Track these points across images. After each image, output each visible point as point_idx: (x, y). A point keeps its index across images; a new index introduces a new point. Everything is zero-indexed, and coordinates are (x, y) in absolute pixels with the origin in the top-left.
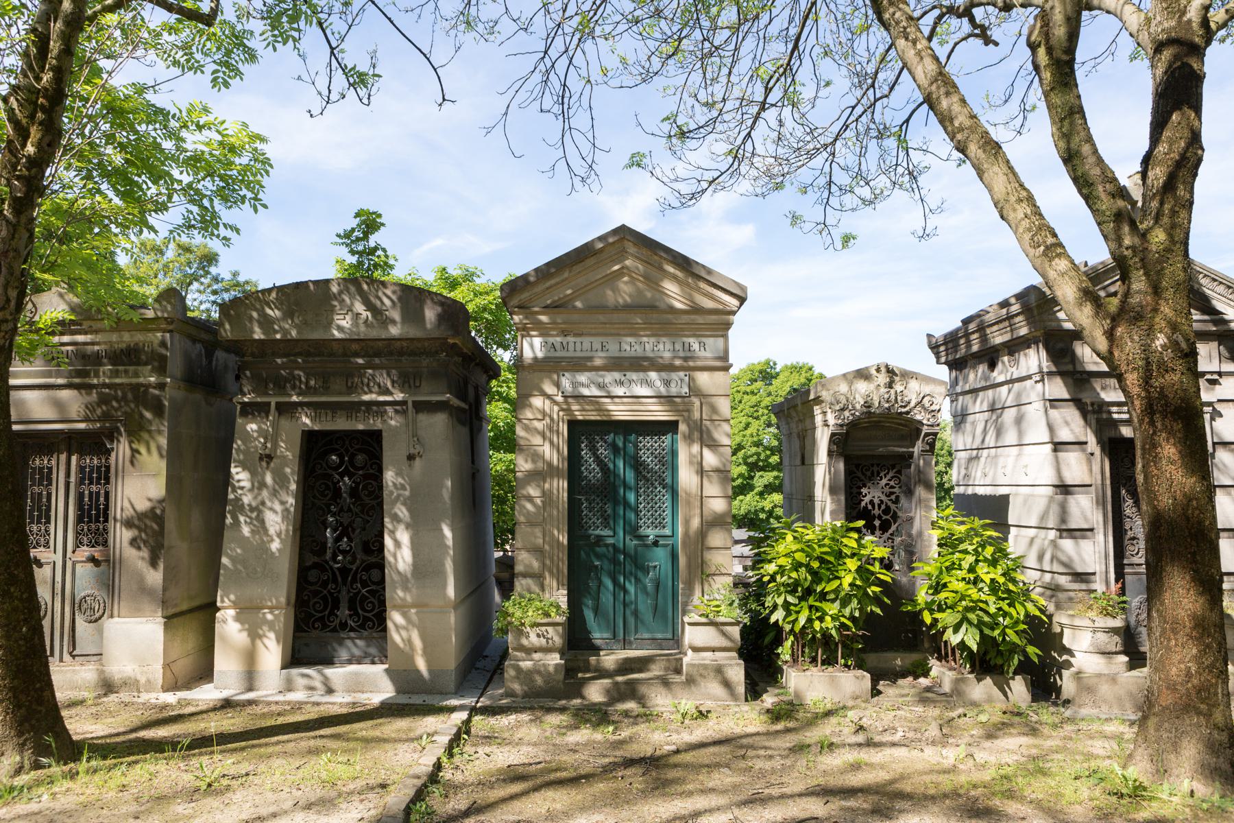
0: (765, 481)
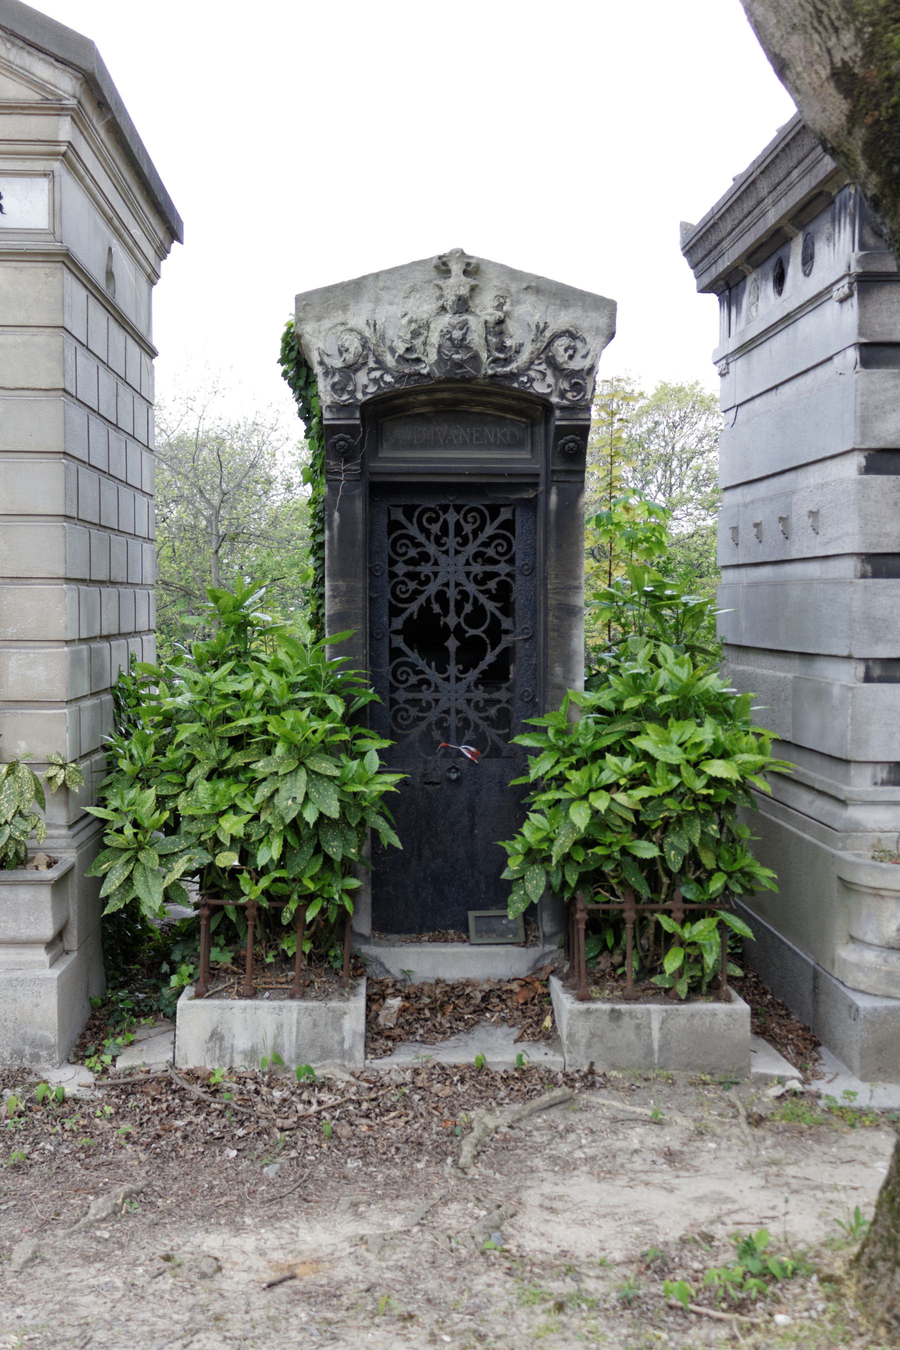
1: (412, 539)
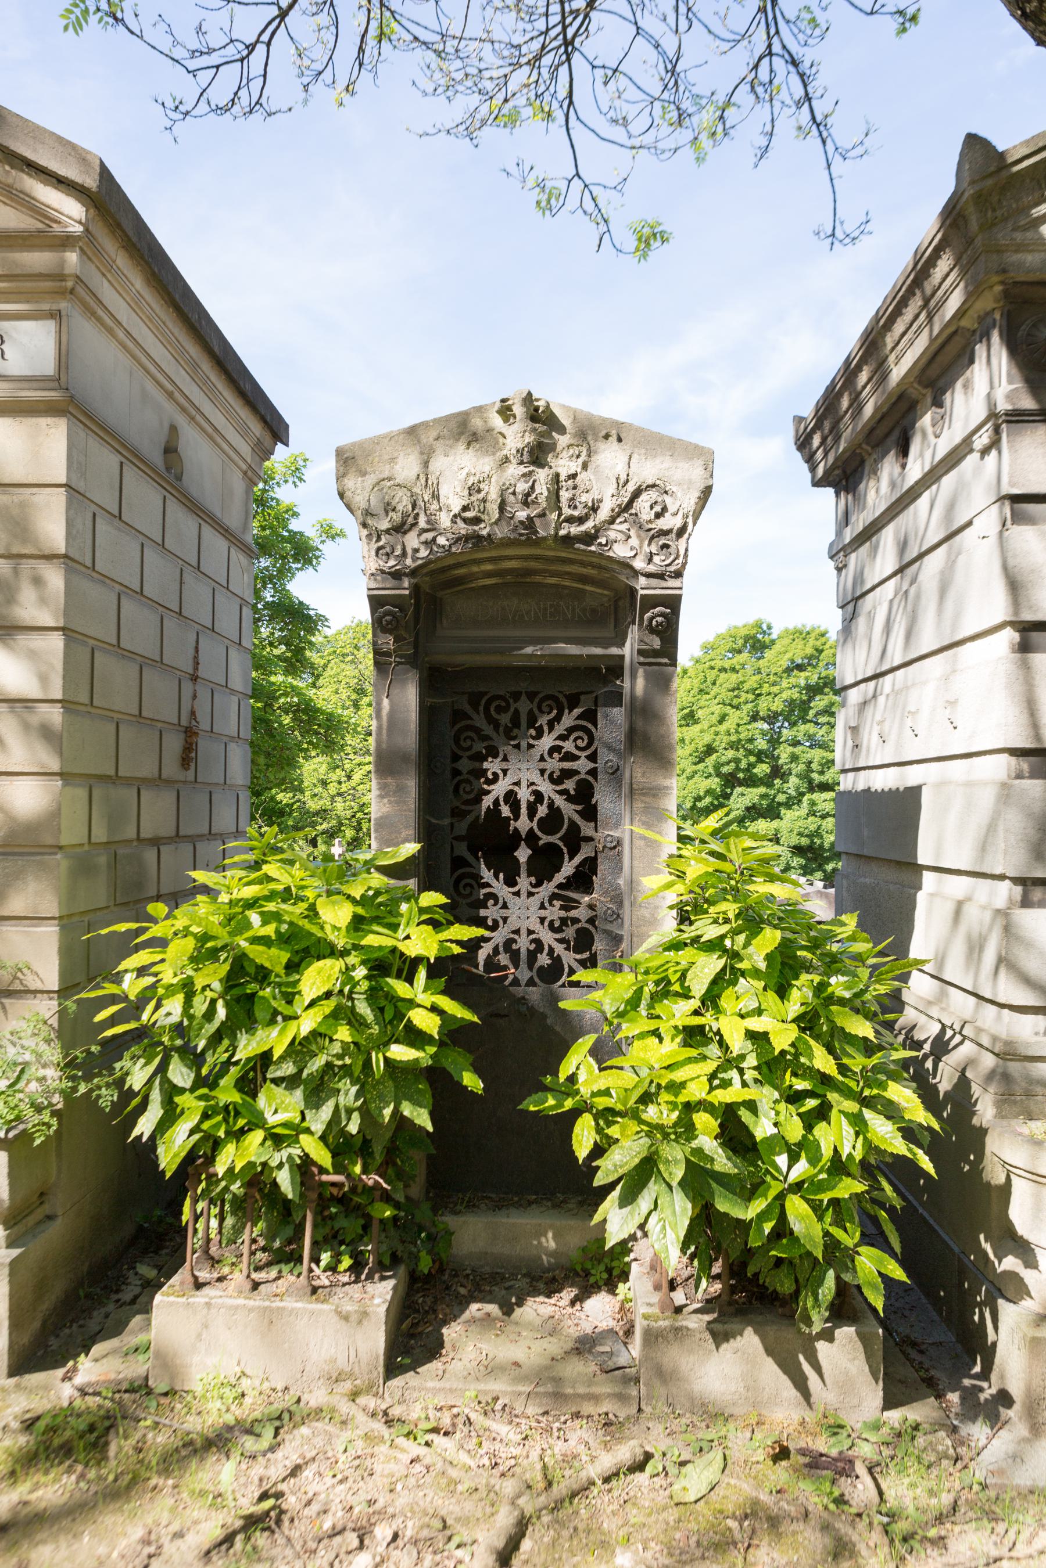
0: (746, 801)
1: (477, 730)
